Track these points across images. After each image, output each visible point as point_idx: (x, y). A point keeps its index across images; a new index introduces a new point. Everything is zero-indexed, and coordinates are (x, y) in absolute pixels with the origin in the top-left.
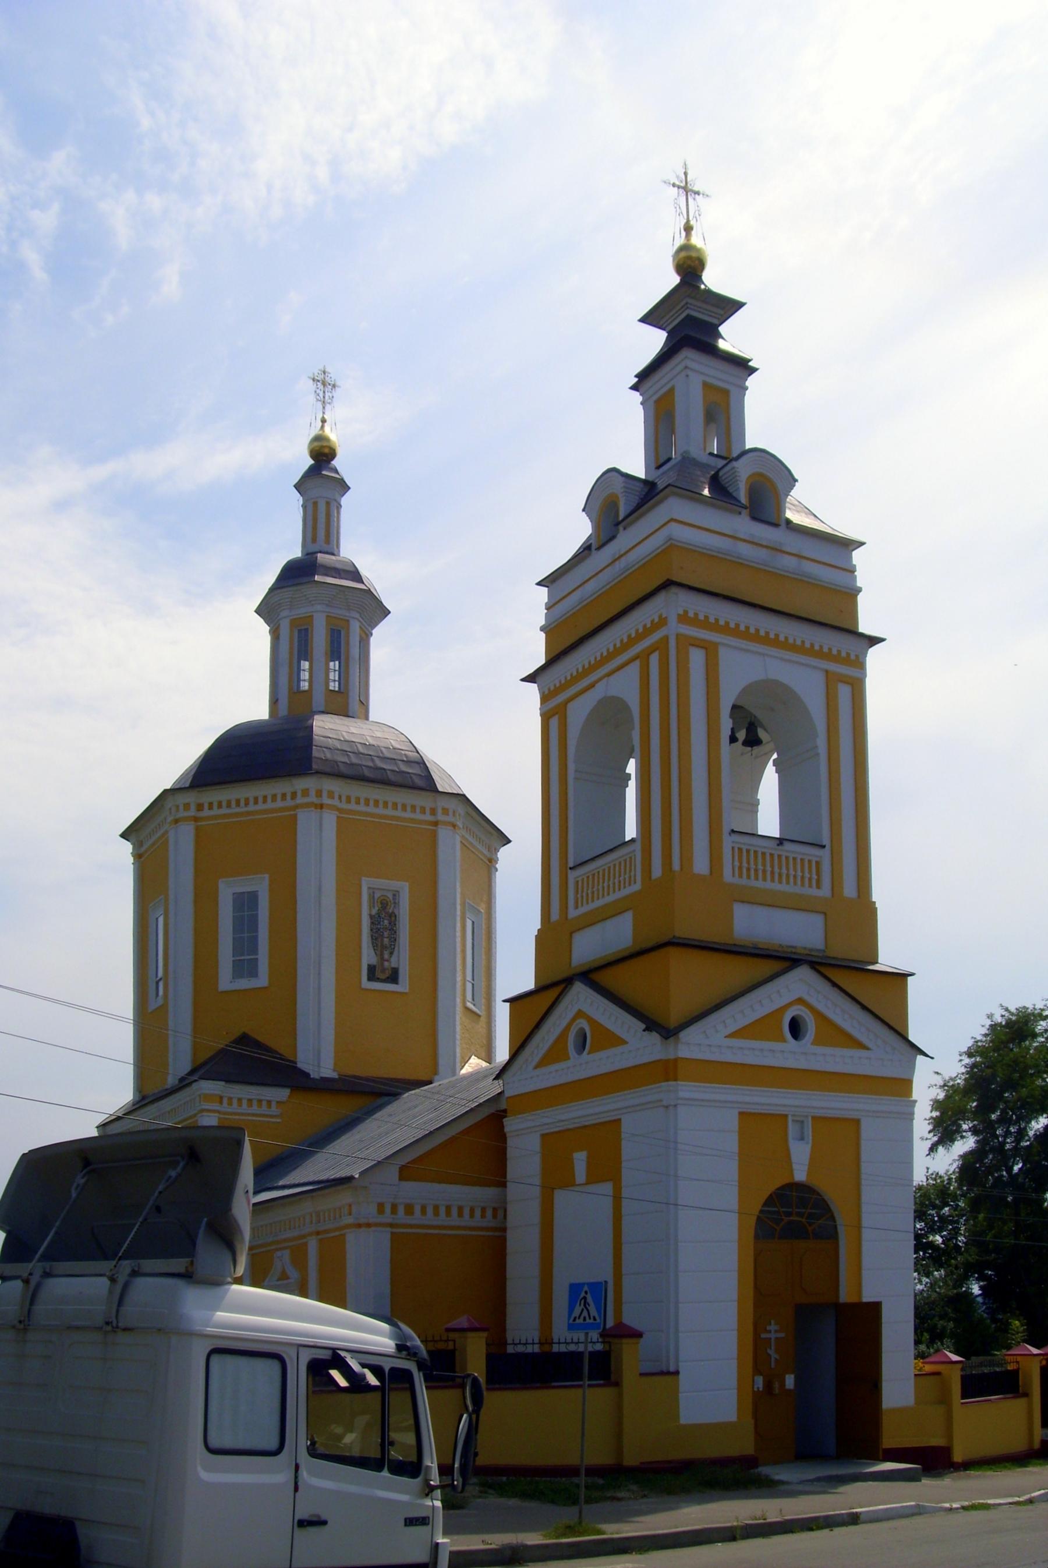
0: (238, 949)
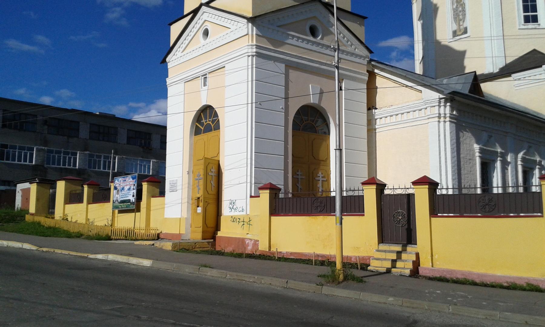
0: (526, 9)
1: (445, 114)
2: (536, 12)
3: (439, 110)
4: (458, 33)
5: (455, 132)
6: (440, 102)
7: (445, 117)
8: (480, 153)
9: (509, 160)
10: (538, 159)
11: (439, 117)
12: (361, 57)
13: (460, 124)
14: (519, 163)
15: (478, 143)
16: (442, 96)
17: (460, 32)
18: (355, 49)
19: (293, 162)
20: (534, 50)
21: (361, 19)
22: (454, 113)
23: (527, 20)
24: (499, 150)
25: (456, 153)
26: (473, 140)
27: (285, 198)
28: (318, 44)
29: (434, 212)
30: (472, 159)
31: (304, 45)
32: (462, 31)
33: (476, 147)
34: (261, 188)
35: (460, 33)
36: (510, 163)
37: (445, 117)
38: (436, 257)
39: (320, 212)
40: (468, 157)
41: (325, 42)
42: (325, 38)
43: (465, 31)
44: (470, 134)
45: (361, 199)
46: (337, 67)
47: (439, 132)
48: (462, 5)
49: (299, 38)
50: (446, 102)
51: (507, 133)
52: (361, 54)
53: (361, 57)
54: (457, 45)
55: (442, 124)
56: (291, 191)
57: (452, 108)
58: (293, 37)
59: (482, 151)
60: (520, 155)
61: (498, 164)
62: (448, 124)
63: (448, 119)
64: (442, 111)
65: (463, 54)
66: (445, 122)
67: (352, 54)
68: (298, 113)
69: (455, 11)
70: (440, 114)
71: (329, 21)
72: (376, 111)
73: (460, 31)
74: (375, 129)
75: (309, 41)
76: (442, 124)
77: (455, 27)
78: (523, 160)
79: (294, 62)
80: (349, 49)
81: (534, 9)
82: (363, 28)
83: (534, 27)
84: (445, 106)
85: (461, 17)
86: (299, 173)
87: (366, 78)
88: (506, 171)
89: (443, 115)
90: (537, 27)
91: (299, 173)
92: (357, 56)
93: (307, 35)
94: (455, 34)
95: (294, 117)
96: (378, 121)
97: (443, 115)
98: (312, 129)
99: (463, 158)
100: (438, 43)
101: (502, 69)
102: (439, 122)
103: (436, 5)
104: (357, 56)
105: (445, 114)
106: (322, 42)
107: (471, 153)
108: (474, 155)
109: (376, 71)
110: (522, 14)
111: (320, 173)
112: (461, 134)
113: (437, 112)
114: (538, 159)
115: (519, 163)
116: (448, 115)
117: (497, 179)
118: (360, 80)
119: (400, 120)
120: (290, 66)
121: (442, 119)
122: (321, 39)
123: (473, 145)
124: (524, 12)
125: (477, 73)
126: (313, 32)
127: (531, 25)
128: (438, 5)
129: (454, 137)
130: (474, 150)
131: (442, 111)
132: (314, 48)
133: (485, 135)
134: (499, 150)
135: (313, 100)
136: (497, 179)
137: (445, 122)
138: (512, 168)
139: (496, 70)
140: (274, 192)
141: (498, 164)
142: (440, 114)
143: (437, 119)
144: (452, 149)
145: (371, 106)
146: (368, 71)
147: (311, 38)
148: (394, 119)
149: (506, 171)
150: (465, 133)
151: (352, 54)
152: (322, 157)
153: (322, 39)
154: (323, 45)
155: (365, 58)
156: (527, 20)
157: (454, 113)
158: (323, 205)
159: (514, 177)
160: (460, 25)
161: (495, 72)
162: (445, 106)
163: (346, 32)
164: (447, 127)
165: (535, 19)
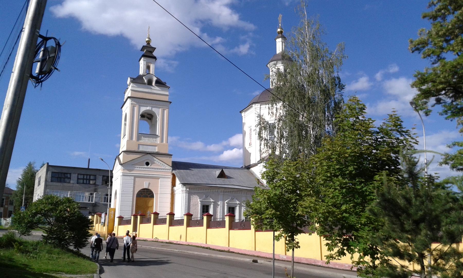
12: (168, 169)
14: (226, 204)
15: (200, 199)
24: (212, 200)
26: (198, 197)
29: (120, 224)
31: (142, 169)
41: (152, 167)
53: (168, 169)
57: (186, 188)
80: (163, 168)
92: (166, 169)
104: (166, 169)
108: (198, 203)
112: (192, 196)
118: (169, 178)
120: (135, 177)
126: (147, 164)
135: (145, 186)
141: (212, 206)
147: (146, 166)
154: (150, 168)
155: (170, 170)
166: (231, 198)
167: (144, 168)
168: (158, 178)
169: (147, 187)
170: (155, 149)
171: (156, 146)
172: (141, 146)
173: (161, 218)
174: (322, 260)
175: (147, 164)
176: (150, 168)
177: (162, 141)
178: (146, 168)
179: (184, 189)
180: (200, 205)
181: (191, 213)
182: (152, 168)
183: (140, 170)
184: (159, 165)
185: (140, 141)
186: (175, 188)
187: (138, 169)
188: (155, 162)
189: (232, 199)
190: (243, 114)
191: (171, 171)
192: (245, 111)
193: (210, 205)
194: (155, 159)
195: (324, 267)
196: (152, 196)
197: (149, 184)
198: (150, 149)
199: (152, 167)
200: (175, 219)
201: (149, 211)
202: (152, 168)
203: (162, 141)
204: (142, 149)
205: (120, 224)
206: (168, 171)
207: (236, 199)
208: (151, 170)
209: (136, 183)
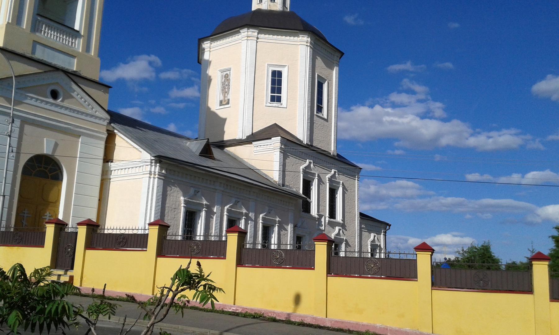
0: (273, 91)
1: (155, 172)
2: (281, 94)
3: (151, 169)
4: (224, 103)
5: (162, 186)
6: (152, 163)
7: (155, 175)
8: (184, 204)
9: (215, 211)
10: (244, 211)
11: (150, 174)
12: (101, 118)
13: (167, 181)
14: (225, 213)
15: (184, 196)
16: (153, 158)
17: (224, 102)
18: (96, 112)
19: (19, 201)
20: (275, 124)
21: (105, 88)
22: (163, 172)
23: (273, 99)
24: (205, 202)
25: (160, 203)
26: (181, 193)
27: (5, 232)
28: (57, 106)
29: (89, 245)
30: (177, 208)
31: (43, 105)
32: (226, 102)
33: (182, 198)
34: (79, 224)
35: (224, 103)
36: (215, 213)
37: (155, 175)
38: (84, 279)
39: (18, 243)
40: (173, 206)
41: (66, 104)
42: (66, 101)
43: (228, 103)
44: (178, 189)
45: (146, 236)
46: (10, 136)
47: (149, 185)
48: (228, 80)
49: (37, 99)
50: (156, 163)
51: (216, 189)
52: (101, 116)
53: (101, 118)
54: (222, 113)
55: (152, 179)
56: (13, 226)
57: (161, 168)
58: (32, 98)
59: (186, 202)
60: (226, 208)
61: (203, 214)
62: (156, 179)
63: (157, 176)
64: (153, 170)
65: (224, 120)
66: (154, 178)
67: (92, 116)
68: (31, 160)
69: (223, 84)
70: (151, 172)
71: (71, 88)
72: (112, 164)
73: (225, 101)
74: (110, 179)
75: (47, 103)
76: (152, 179)
77: (222, 98)
78: (228, 211)
79: (30, 119)
80: (89, 112)
81: (279, 91)
82: (107, 96)
83: (277, 105)
84: (156, 166)
85: (226, 90)
86: (26, 212)
87: (105, 136)
88: (211, 219)
89: (153, 173)
90: (280, 106)
91: (26, 212)
92: (96, 117)
93: (47, 97)
94: (221, 103)
95: (26, 163)
96: (113, 172)
97: (153, 173)
98: (44, 175)
99: (169, 207)
100: (209, 109)
101: (248, 137)
102: (150, 177)
103: (210, 77)
104: (96, 117)
105: (155, 172)
106: (62, 104)
107: (177, 203)
108: (179, 205)
109: (115, 131)
110: (270, 94)
111: (48, 213)
112: (169, 188)
113: (149, 170)
114: (244, 211)
115: (225, 213)
116: (157, 173)
117: (201, 225)
118: (99, 138)
119: (126, 173)
120: (25, 121)
121: (152, 176)
122: (61, 101)
123: (179, 197)
124: (271, 93)
125: (210, 141)
126: (55, 95)
127: (275, 104)
128: (212, 78)
129: (161, 190)
130: (180, 201)
131: (153, 170)
132: (53, 108)
133: (192, 191)
134: (205, 202)
135: (46, 150)
136: (201, 225)
137: (154, 178)
138: (217, 217)
139: (244, 138)
140: (60, 226)
141: (203, 214)
142: (151, 172)
143: (148, 175)
144: (157, 200)
145: (108, 158)
146: (108, 130)
147: (51, 100)
148: (123, 172)
149: (211, 219)
150: (173, 187)
151: (92, 116)
152: (52, 198)
153: (62, 101)
154: (62, 107)
155: (104, 120)
156: (273, 99)
157: (163, 172)
158: (125, 241)
159: (218, 224)
160: (225, 97)
161: (244, 138)
162: (156, 166)
163: (87, 98)
164: (156, 182)
165: (279, 99)
166: (234, 200)
167: (47, 103)
168: (78, 135)
169: (50, 153)
170: (71, 64)
171: (74, 57)
172: (38, 47)
173: (110, 232)
174: (234, 304)
175: (55, 95)
176: (62, 107)
177: (87, 48)
178: (52, 104)
179: (157, 169)
180: (183, 210)
181: (100, 224)
182: (67, 108)
183: (36, 107)
184: (81, 105)
185: (38, 34)
186: (112, 165)
187: (33, 102)
188: (74, 94)
189: (235, 205)
190: (206, 45)
191: (105, 123)
192: (213, 40)
193: (200, 211)
194: (74, 86)
195: (117, 300)
196: (58, 178)
197: (56, 145)
198: (59, 61)
199: (66, 104)
200: (168, 238)
201: (47, 214)
202: (67, 108)
203: (87, 48)
204: (41, 54)
205: (89, 245)
206: (101, 122)
207: (243, 204)
208: (62, 111)
209: (24, 137)
